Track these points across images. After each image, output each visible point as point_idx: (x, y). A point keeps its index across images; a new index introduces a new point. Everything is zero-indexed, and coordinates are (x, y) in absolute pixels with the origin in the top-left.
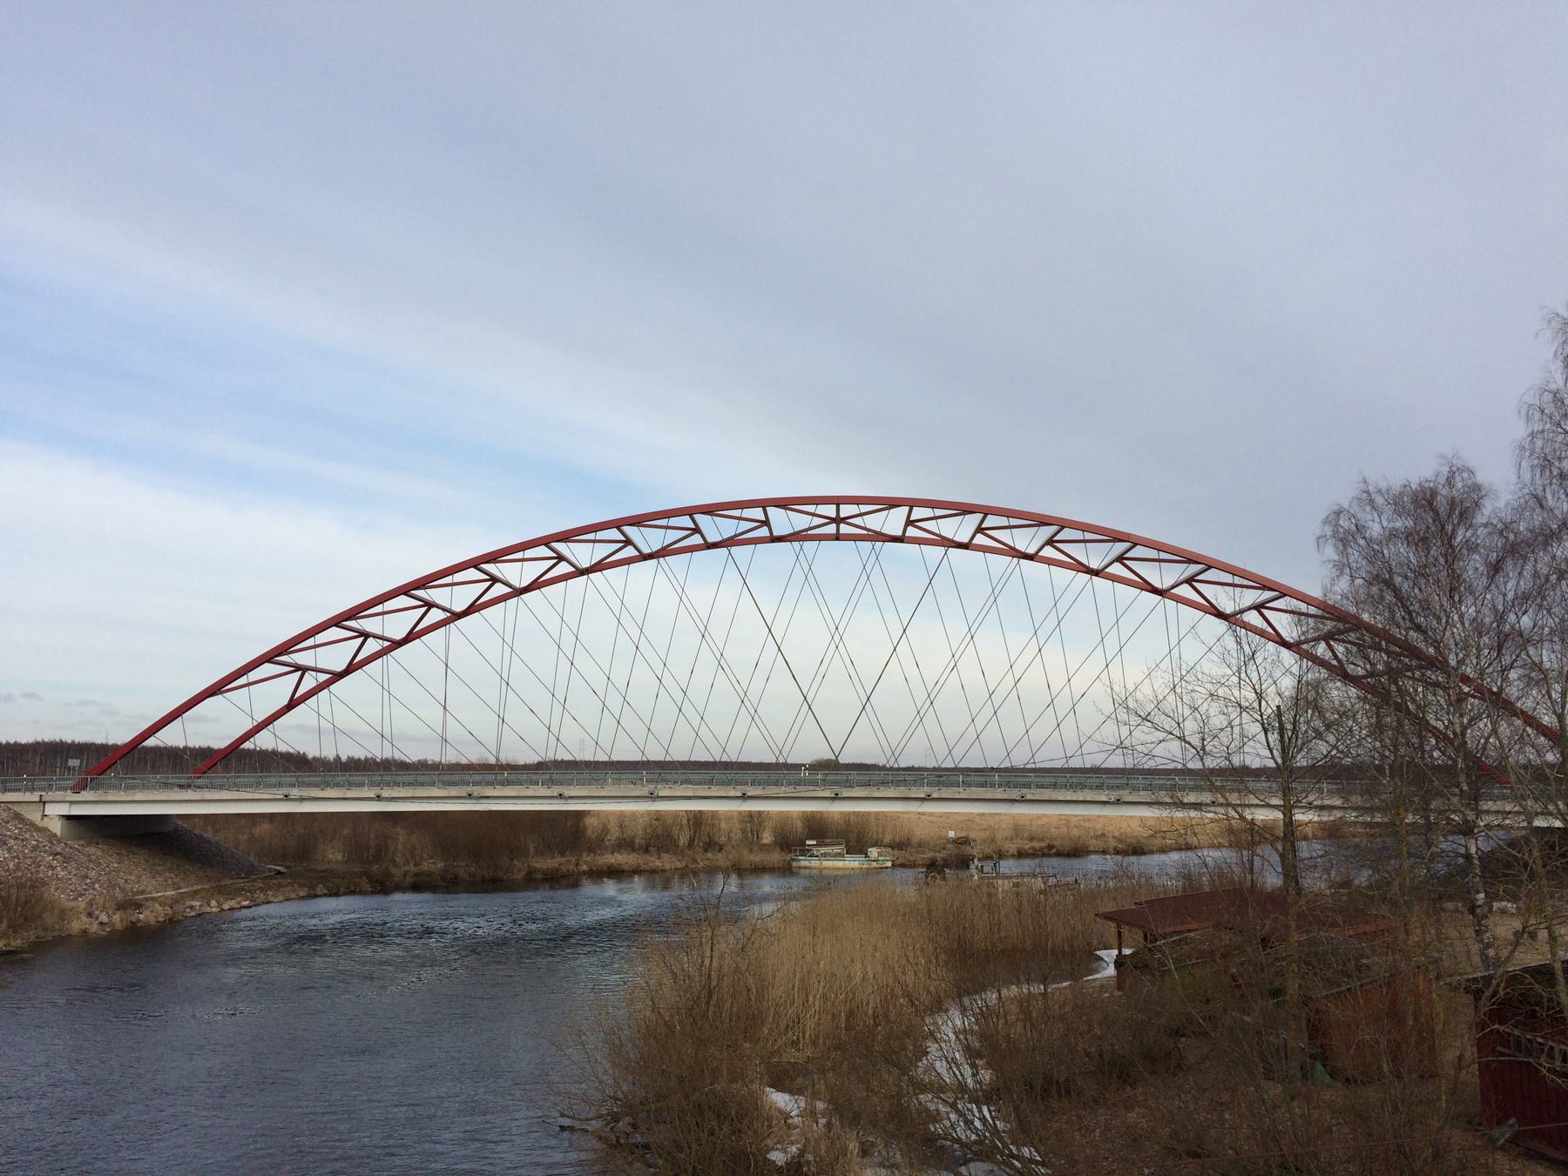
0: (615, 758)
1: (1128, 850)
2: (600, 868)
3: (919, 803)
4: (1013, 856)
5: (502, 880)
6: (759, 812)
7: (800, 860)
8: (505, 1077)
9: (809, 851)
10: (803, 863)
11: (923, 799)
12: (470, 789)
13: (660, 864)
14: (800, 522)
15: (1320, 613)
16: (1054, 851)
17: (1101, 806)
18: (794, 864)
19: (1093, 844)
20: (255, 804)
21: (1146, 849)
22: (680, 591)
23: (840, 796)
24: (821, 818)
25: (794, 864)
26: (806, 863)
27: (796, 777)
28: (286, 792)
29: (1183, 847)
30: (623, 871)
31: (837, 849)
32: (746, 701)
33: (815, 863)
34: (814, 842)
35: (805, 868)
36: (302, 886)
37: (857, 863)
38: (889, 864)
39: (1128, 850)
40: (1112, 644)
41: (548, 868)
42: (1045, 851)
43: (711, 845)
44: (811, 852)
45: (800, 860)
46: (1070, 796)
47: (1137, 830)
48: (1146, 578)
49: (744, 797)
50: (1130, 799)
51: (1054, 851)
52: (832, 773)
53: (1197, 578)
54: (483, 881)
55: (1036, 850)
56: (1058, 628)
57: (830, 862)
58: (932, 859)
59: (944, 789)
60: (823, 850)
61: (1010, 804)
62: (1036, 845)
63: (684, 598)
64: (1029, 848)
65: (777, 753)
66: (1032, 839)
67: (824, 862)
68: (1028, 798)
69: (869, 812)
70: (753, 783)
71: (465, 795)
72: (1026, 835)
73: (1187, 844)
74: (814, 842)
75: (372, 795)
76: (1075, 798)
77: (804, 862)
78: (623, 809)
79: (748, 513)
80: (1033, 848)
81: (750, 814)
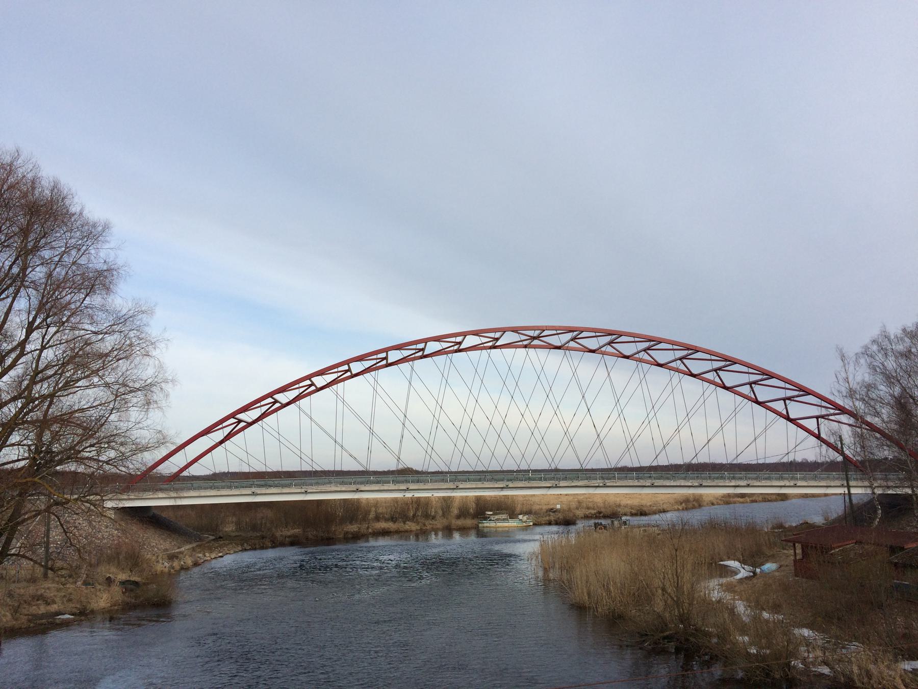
0: (490, 469)
1: (638, 513)
2: (378, 530)
3: (779, 488)
4: (582, 518)
5: (333, 538)
6: (466, 496)
7: (483, 523)
8: (23, 663)
9: (489, 517)
10: (485, 525)
11: (502, 488)
12: (253, 489)
13: (409, 528)
14: (329, 378)
15: (71, 328)
16: (602, 515)
17: (594, 488)
18: (480, 525)
19: (580, 513)
20: (264, 496)
21: (666, 510)
22: (574, 371)
23: (558, 485)
24: (497, 502)
25: (480, 525)
26: (488, 525)
27: (527, 476)
28: (306, 490)
29: (662, 510)
30: (391, 532)
31: (504, 516)
32: (567, 433)
33: (492, 524)
34: (492, 513)
35: (487, 527)
36: (237, 545)
37: (515, 523)
38: (531, 524)
39: (638, 513)
40: (511, 384)
41: (354, 531)
42: (598, 515)
43: (427, 516)
44: (490, 518)
45: (483, 523)
46: (673, 483)
47: (647, 502)
48: (548, 341)
49: (254, 494)
50: (311, 491)
51: (602, 515)
52: (405, 474)
53: (541, 335)
54: (322, 539)
55: (592, 515)
56: (640, 385)
57: (501, 523)
58: (549, 521)
59: (641, 481)
60: (497, 517)
61: (688, 488)
62: (593, 512)
63: (575, 374)
64: (589, 514)
65: (550, 460)
66: (588, 508)
67: (498, 524)
68: (460, 487)
69: (508, 495)
70: (413, 482)
71: (251, 493)
72: (585, 505)
73: (663, 509)
74: (492, 513)
75: (792, 484)
76: (675, 485)
77: (486, 524)
78: (396, 496)
79: (341, 369)
80: (590, 513)
81: (444, 498)
